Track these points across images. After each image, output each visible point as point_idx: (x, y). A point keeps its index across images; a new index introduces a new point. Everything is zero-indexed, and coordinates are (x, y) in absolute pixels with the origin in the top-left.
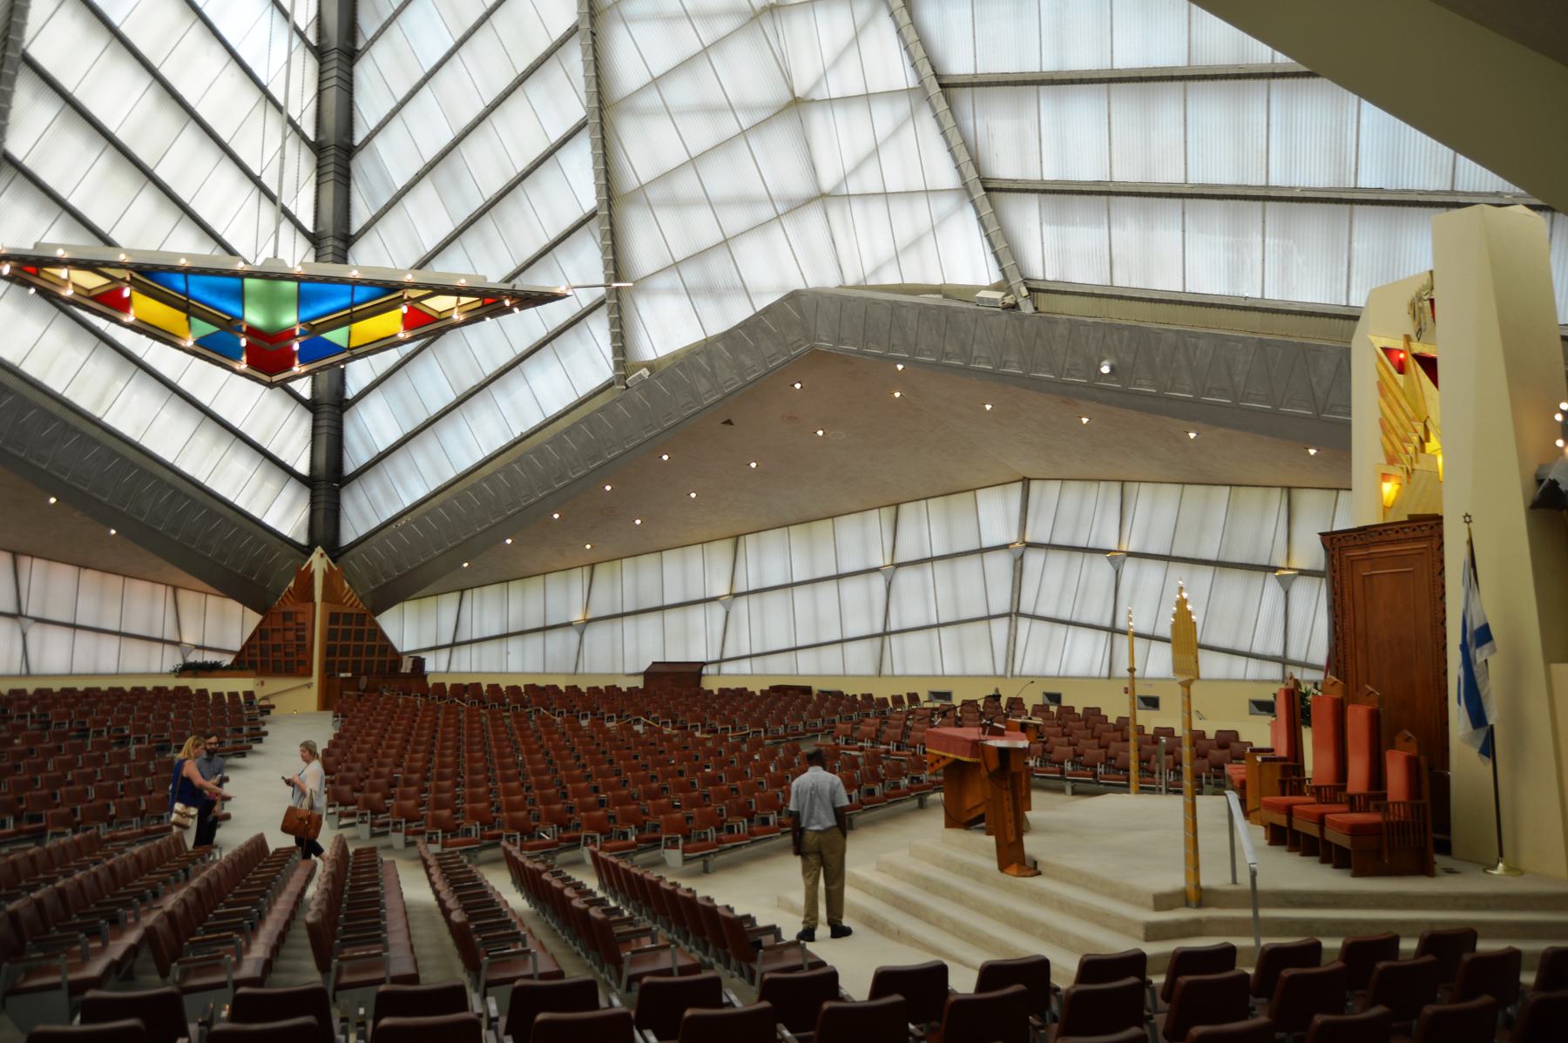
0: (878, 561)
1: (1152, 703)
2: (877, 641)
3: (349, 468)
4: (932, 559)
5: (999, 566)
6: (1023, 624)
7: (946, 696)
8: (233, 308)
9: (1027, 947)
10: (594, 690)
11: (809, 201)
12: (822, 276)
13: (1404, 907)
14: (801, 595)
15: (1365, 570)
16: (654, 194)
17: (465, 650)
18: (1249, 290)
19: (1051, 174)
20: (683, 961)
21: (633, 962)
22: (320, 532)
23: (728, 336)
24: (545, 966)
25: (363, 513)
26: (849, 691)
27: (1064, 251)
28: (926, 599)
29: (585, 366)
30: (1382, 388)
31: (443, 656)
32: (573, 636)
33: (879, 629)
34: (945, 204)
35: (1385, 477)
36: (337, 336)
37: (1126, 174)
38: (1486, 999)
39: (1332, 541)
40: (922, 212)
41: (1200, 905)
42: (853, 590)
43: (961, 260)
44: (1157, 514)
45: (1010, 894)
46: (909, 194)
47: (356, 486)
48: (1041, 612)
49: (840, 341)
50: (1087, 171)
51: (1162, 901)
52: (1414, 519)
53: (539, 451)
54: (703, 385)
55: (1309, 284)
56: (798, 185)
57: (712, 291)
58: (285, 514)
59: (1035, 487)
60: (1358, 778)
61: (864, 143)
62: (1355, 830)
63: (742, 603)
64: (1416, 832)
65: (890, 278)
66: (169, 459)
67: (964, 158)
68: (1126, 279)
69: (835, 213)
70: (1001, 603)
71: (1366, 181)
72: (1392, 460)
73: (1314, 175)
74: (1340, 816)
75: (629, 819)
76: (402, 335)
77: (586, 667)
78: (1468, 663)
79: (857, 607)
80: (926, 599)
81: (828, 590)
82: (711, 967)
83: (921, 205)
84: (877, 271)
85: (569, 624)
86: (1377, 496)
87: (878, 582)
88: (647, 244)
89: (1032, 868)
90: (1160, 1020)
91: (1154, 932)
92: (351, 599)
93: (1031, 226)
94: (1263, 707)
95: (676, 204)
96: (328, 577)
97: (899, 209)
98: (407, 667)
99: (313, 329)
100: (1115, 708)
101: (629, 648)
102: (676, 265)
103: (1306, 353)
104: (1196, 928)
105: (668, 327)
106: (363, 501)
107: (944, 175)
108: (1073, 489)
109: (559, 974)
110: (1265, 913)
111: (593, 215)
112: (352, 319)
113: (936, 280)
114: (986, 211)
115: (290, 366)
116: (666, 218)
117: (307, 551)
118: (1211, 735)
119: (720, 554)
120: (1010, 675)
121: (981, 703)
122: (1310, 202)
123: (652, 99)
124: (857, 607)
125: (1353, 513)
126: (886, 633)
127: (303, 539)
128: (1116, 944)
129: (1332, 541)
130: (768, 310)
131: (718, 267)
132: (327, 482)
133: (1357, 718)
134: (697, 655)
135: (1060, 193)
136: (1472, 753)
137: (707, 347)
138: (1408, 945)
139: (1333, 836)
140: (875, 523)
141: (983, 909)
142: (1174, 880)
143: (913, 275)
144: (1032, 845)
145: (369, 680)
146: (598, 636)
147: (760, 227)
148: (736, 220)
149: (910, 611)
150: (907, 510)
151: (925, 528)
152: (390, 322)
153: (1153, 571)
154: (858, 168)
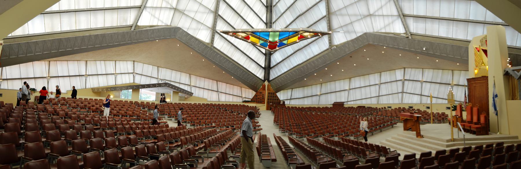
0: (377, 83)
1: (428, 108)
3: (272, 66)
5: (400, 83)
6: (404, 94)
7: (390, 107)
8: (267, 38)
9: (427, 150)
10: (323, 108)
11: (368, 16)
12: (370, 30)
13: (483, 140)
14: (363, 89)
15: (474, 85)
16: (337, 13)
17: (293, 100)
18: (450, 36)
19: (415, 13)
20: (329, 160)
21: (319, 160)
22: (266, 78)
23: (352, 41)
24: (301, 162)
25: (274, 74)
26: (373, 107)
27: (417, 28)
29: (323, 45)
30: (475, 54)
31: (289, 101)
32: (318, 97)
33: (378, 95)
34: (395, 18)
35: (475, 69)
36: (285, 42)
37: (429, 14)
38: (474, 158)
39: (469, 80)
40: (390, 19)
41: (454, 141)
42: (373, 88)
43: (398, 28)
44: (429, 74)
45: (419, 141)
46: (388, 16)
47: (273, 69)
48: (408, 92)
49: (374, 42)
50: (422, 14)
51: (448, 141)
52: (483, 77)
53: (313, 62)
54: (347, 50)
55: (461, 36)
56: (366, 13)
57: (348, 32)
58: (260, 74)
59: (406, 69)
60: (475, 119)
61: (379, 5)
62: (477, 128)
63: (351, 91)
64: (484, 129)
65: (383, 31)
66: (242, 65)
67: (399, 10)
68: (428, 33)
69: (373, 18)
70: (400, 90)
71: (471, 19)
72: (477, 66)
73: (462, 17)
74: (473, 126)
75: (312, 132)
76: (298, 41)
77: (321, 103)
78: (494, 100)
79: (374, 91)
81: (368, 88)
82: (334, 160)
83: (390, 18)
84: (381, 29)
85: (317, 95)
86: (474, 72)
87: (377, 87)
88: (336, 22)
89: (422, 137)
90: (418, 166)
91: (448, 146)
92: (272, 90)
93: (411, 23)
94: (449, 108)
95: (342, 15)
96: (268, 86)
97: (386, 18)
98: (282, 103)
99: (281, 41)
100: (423, 109)
101: (329, 99)
102: (341, 27)
103: (460, 47)
104: (454, 145)
105: (339, 39)
106: (274, 72)
107: (395, 13)
108: (413, 70)
109: (304, 163)
110: (466, 142)
111: (325, 16)
112: (289, 39)
113: (392, 32)
114: (403, 20)
115: (276, 48)
116: (340, 18)
117: (264, 81)
118: (440, 113)
119: (347, 81)
120: (402, 103)
122: (469, 24)
124: (374, 91)
125: (471, 76)
127: (263, 79)
128: (442, 148)
129: (469, 80)
130: (360, 36)
131: (350, 28)
132: (268, 68)
133: (475, 110)
134: (343, 101)
135: (417, 17)
136: (494, 115)
137: (348, 43)
138: (484, 146)
139: (472, 129)
140: (377, 75)
141: (415, 144)
142: (449, 137)
143: (388, 31)
144: (422, 133)
145: (276, 106)
146: (323, 97)
147: (358, 20)
148: (353, 19)
149: (383, 92)
150: (383, 73)
151: (386, 77)
152: (296, 39)
153: (428, 85)
154: (378, 10)
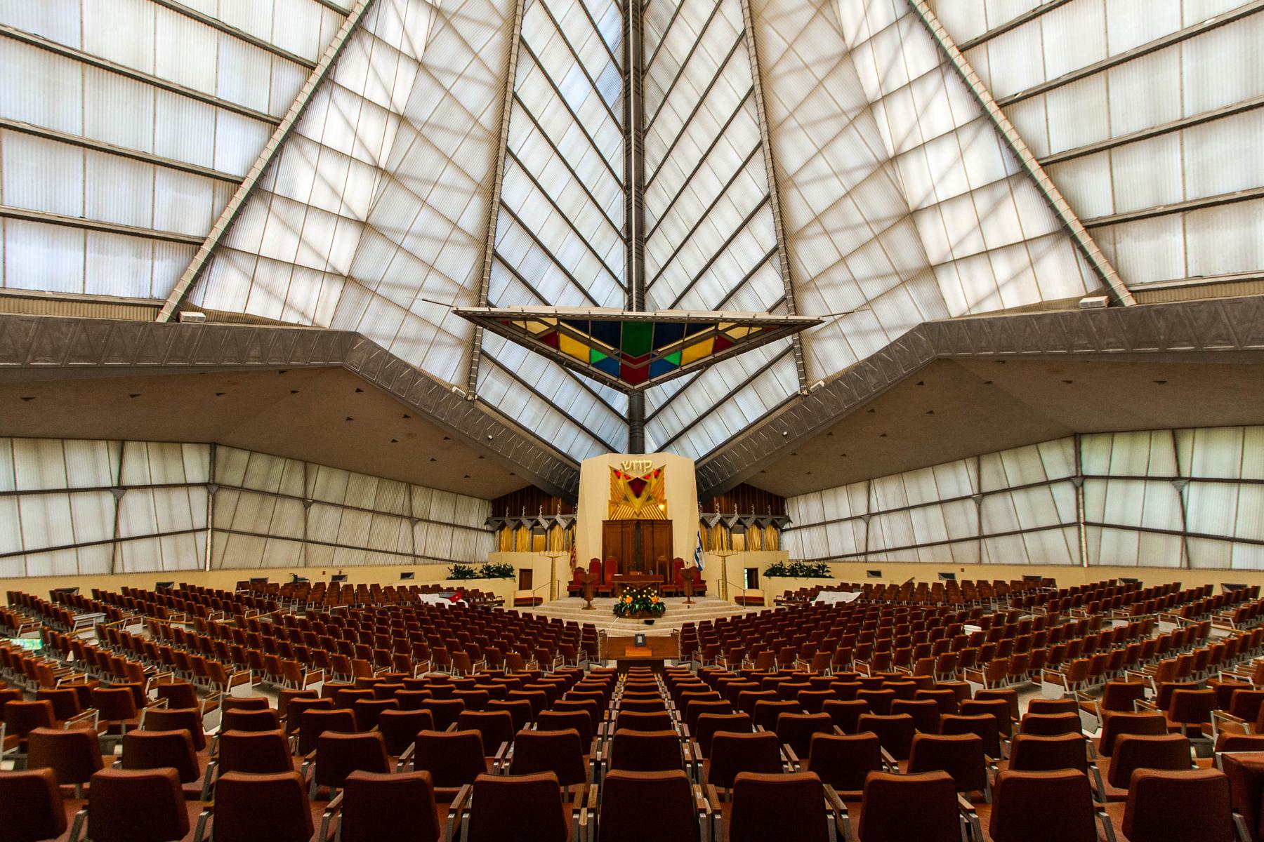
2: (111, 546)
4: (152, 486)
14: (28, 504)
28: (150, 516)
33: (110, 536)
42: (84, 504)
80: (150, 516)
121: (930, 587)
123: (312, 152)
126: (116, 541)
137: (859, 368)
148: (307, 259)
150: (131, 447)
